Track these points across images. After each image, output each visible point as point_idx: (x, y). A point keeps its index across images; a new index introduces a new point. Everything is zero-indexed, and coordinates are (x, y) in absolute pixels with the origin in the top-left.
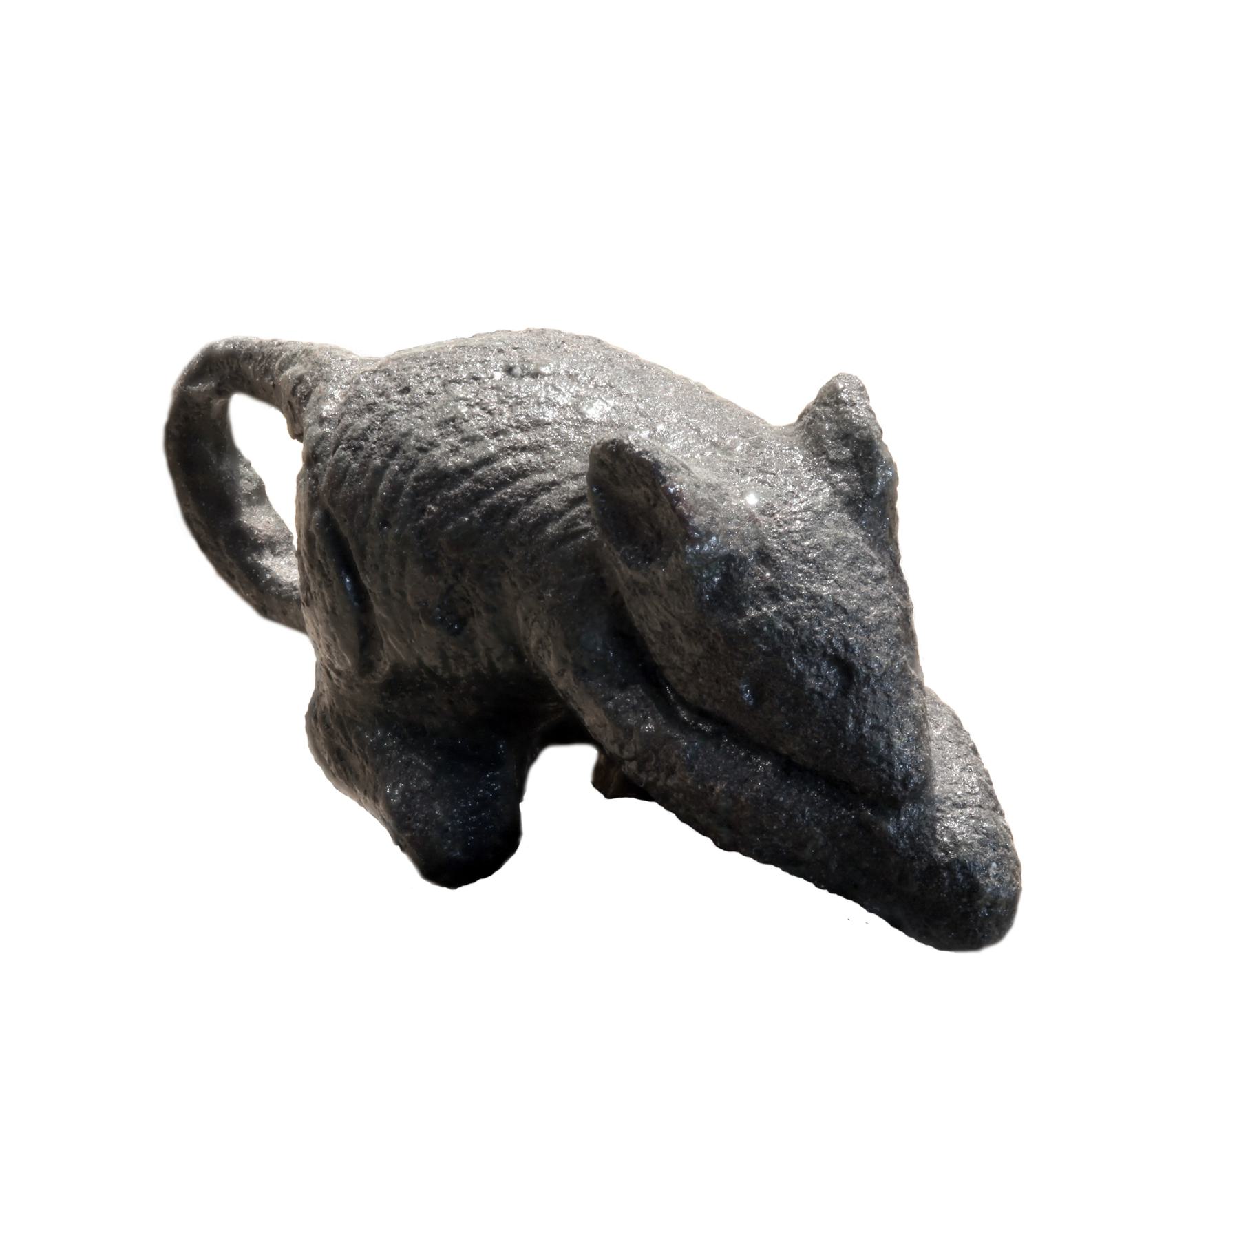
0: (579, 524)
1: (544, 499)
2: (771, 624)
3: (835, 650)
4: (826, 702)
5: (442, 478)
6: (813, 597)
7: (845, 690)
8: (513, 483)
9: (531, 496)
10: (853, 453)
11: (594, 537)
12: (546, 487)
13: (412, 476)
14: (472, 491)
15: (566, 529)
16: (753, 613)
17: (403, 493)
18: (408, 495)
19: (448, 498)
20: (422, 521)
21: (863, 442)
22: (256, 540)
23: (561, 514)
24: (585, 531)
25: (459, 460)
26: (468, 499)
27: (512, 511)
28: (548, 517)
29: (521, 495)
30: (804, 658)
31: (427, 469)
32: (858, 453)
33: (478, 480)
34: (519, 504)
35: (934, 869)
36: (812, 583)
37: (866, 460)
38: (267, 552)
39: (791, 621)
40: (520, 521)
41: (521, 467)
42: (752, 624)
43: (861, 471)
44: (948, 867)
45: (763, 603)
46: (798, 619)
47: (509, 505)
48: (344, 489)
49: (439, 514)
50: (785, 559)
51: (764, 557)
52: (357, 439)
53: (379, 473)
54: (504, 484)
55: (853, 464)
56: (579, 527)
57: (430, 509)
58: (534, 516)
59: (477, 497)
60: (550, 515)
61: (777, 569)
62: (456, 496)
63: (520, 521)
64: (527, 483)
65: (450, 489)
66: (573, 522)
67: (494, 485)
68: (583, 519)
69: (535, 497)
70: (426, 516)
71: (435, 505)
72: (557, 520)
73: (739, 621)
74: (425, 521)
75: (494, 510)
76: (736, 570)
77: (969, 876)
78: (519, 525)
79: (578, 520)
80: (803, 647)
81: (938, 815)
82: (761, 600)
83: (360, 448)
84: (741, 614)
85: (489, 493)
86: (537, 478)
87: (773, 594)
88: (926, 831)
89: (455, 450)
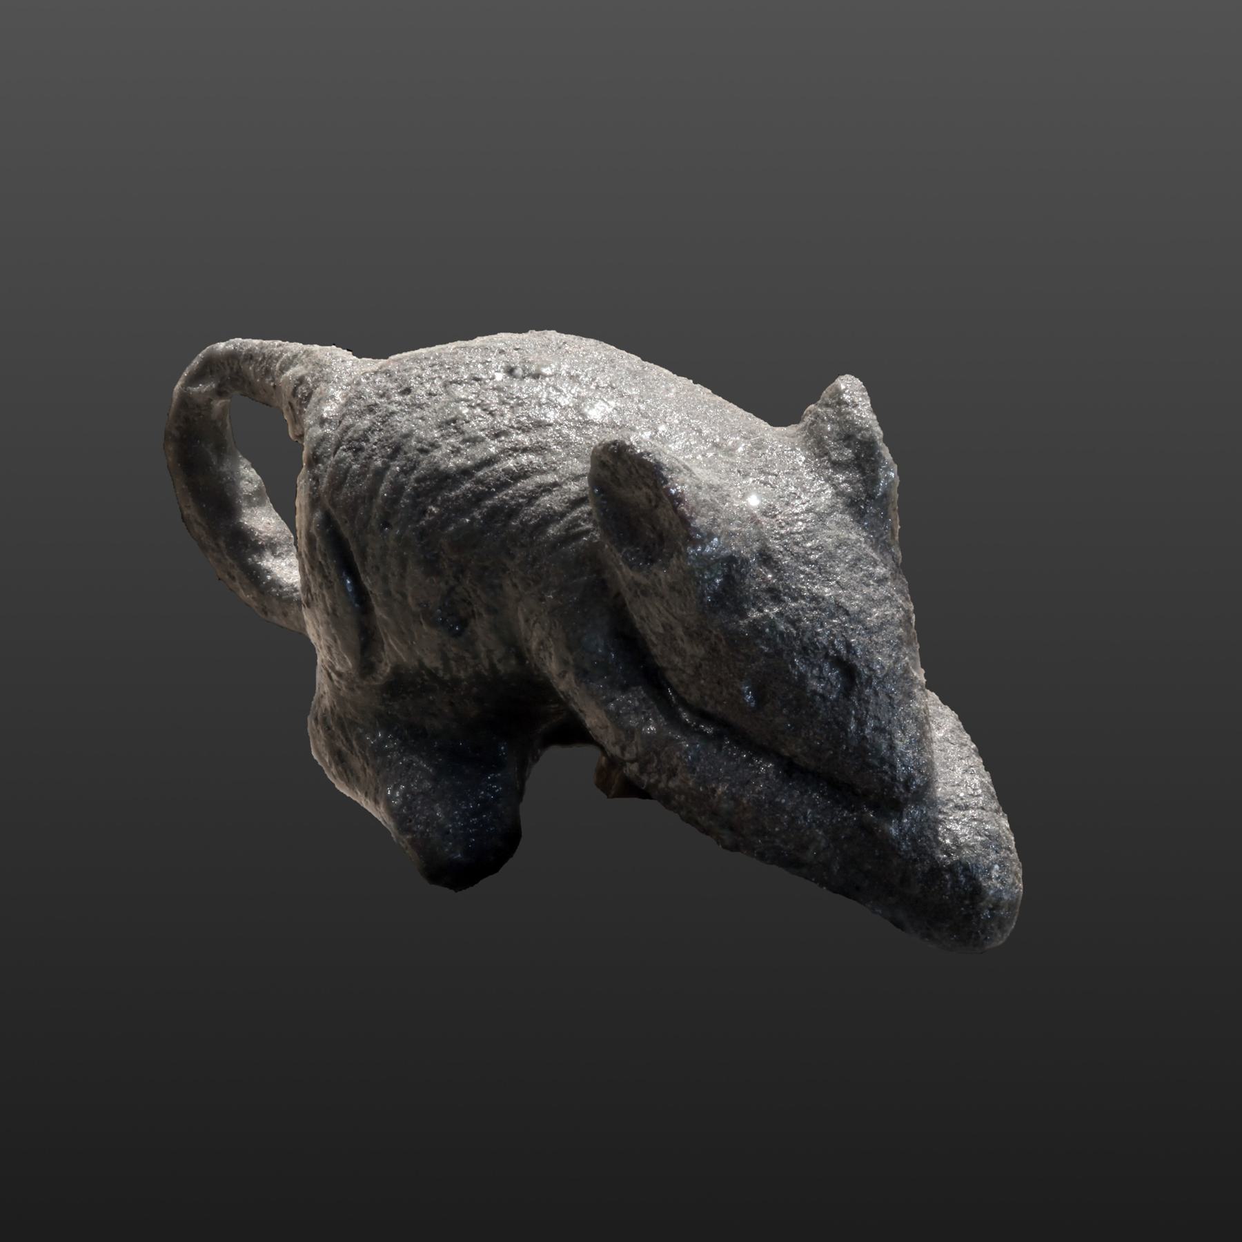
0: (580, 525)
1: (546, 500)
2: (772, 625)
3: (837, 651)
4: (828, 704)
5: (443, 479)
6: (815, 598)
7: (847, 692)
9: (532, 498)
10: (856, 454)
11: (596, 538)
12: (547, 489)
13: (413, 477)
14: (473, 492)
15: (567, 530)
16: (755, 615)
17: (404, 494)
18: (409, 496)
19: (449, 500)
20: (423, 523)
21: (865, 443)
22: (257, 541)
23: (563, 515)
24: (587, 532)
25: (460, 461)
26: (469, 501)
27: (513, 512)
28: (549, 518)
29: (522, 496)
30: (806, 659)
31: (428, 470)
32: (860, 454)
33: (480, 482)
34: (520, 505)
35: (936, 871)
36: (814, 584)
37: (868, 461)
38: (268, 553)
39: (793, 623)
40: (521, 522)
41: (523, 468)
42: (754, 625)
43: (863, 472)
44: (951, 869)
45: (765, 605)
47: (510, 507)
48: (344, 490)
49: (440, 515)
50: (787, 560)
51: (766, 558)
52: (357, 440)
53: (380, 474)
55: (855, 465)
56: (581, 528)
57: (431, 510)
58: (536, 517)
59: (479, 498)
60: (552, 516)
61: (779, 570)
62: (457, 497)
63: (521, 522)
64: (528, 484)
65: (451, 491)
66: (575, 523)
67: (495, 486)
68: (585, 521)
69: (537, 498)
70: (427, 518)
71: (436, 506)
72: (558, 522)
73: (741, 622)
74: (426, 522)
75: (495, 512)
76: (738, 571)
77: (972, 878)
78: (520, 526)
79: (579, 521)
80: (805, 649)
81: (941, 817)
82: (763, 602)
83: (361, 449)
84: (743, 615)
85: (490, 495)
86: (538, 479)
87: (775, 595)
88: (928, 833)
89: (456, 451)
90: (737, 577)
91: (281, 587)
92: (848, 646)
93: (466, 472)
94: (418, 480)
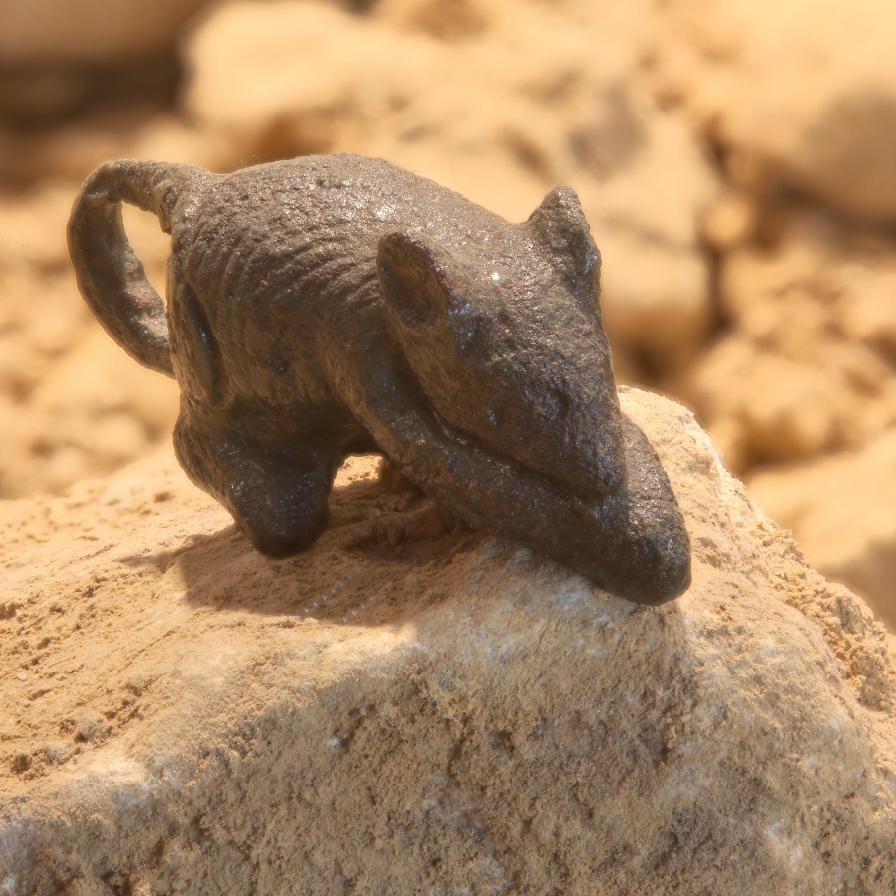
1: (346, 276)
2: (509, 367)
4: (550, 423)
5: (271, 261)
6: (540, 347)
7: (563, 414)
8: (323, 264)
9: (336, 274)
10: (569, 243)
12: (346, 268)
14: (293, 270)
15: (361, 298)
16: (497, 359)
19: (276, 276)
20: (257, 292)
24: (375, 299)
25: (284, 248)
27: (322, 285)
29: (328, 273)
33: (298, 263)
34: (327, 280)
35: (627, 544)
38: (145, 315)
39: (524, 365)
40: (328, 292)
43: (575, 256)
44: (638, 542)
45: (504, 351)
46: (529, 363)
48: (200, 269)
50: (520, 319)
51: (504, 318)
53: (226, 257)
54: (317, 265)
59: (297, 275)
62: (282, 274)
63: (328, 292)
65: (277, 269)
66: (367, 292)
68: (374, 291)
69: (339, 275)
72: (355, 292)
73: (487, 364)
75: (309, 284)
76: (484, 327)
81: (631, 504)
82: (502, 350)
83: (212, 239)
84: (488, 358)
85: (306, 272)
86: (340, 261)
87: (511, 345)
88: (622, 516)
89: (281, 241)
90: (484, 331)
91: (155, 339)
92: (564, 381)
93: (288, 256)
94: (254, 262)
